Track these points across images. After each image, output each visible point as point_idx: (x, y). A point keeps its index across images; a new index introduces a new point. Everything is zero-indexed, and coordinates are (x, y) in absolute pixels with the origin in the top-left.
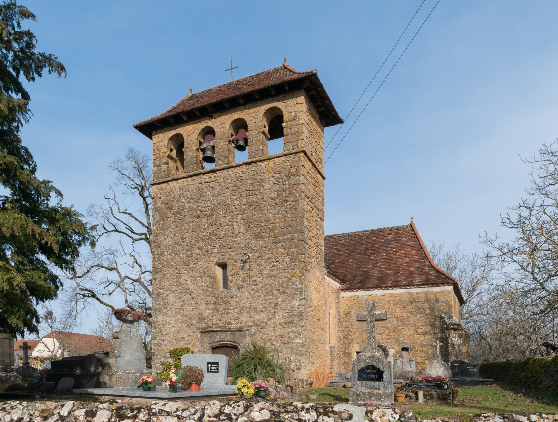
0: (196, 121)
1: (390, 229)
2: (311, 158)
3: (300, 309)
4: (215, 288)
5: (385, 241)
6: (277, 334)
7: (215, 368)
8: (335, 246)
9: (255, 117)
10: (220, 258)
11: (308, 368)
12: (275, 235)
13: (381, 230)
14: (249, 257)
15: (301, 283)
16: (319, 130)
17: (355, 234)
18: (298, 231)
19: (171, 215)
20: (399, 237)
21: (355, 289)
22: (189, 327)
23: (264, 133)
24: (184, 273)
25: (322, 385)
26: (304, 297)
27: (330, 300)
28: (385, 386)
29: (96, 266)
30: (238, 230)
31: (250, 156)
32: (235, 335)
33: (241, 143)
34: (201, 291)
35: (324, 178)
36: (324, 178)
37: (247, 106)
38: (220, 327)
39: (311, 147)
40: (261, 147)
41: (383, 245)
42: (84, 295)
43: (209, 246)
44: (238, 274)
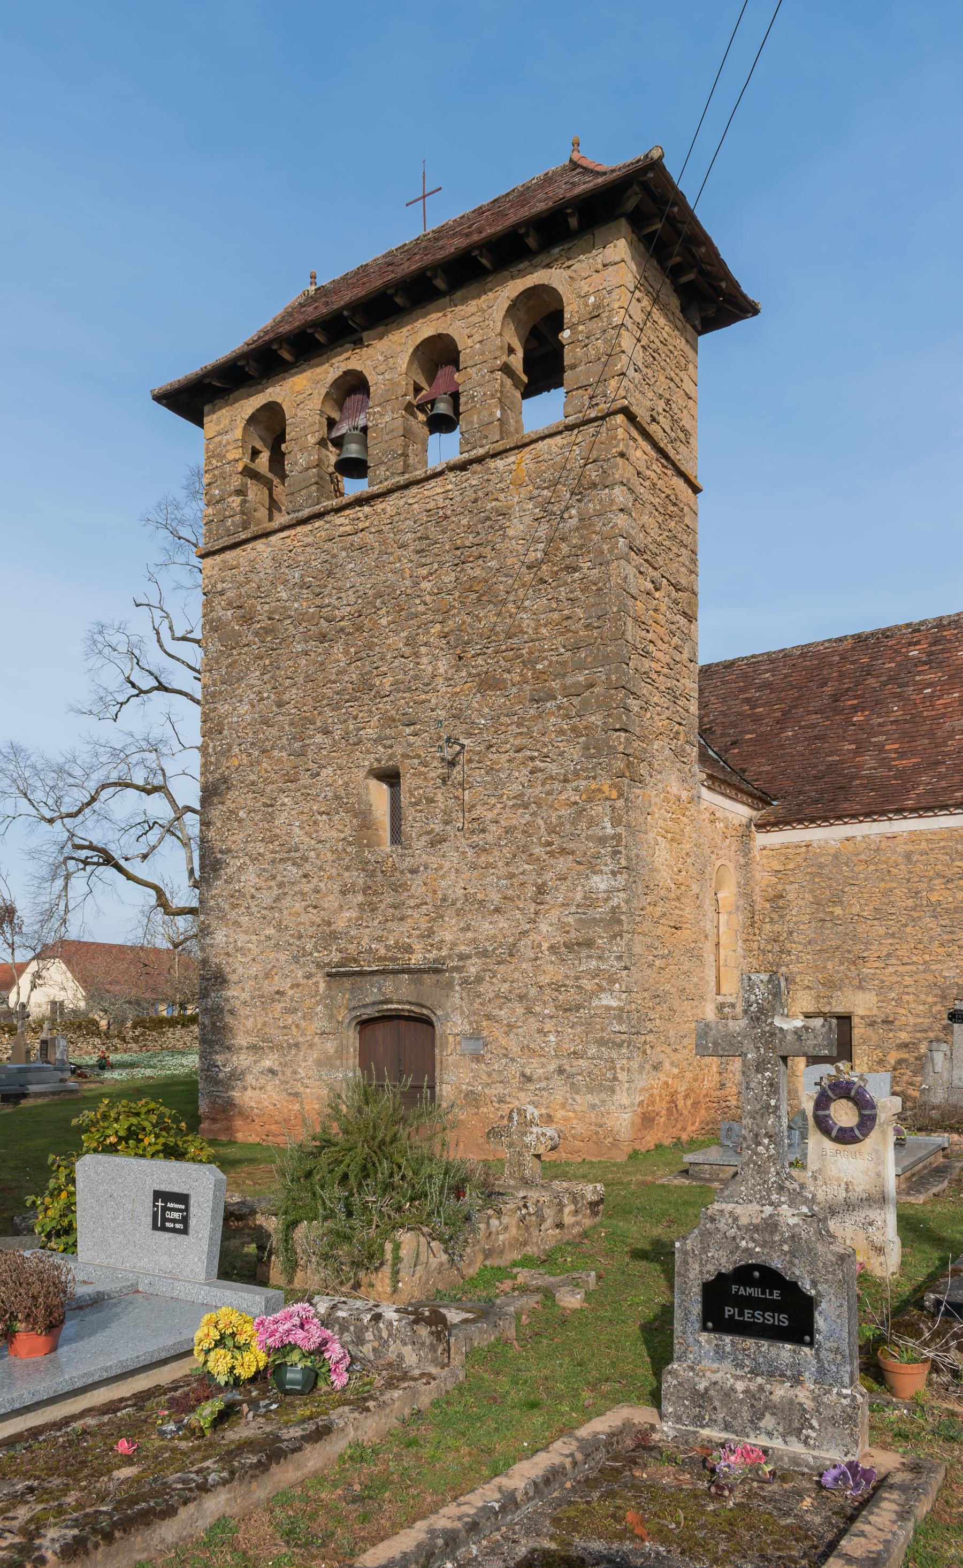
0: (317, 360)
1: (915, 628)
2: (653, 428)
3: (611, 903)
4: (368, 846)
5: (899, 665)
6: (544, 980)
7: (176, 1215)
8: (742, 690)
9: (481, 324)
10: (380, 756)
11: (641, 1084)
12: (538, 676)
13: (886, 634)
14: (463, 746)
15: (616, 822)
16: (681, 343)
17: (805, 652)
18: (605, 660)
19: (250, 638)
20: (943, 651)
21: (800, 821)
22: (296, 960)
23: (506, 369)
24: (283, 804)
25: (690, 1128)
26: (624, 863)
27: (719, 863)
28: (822, 1371)
29: (115, 784)
30: (430, 669)
31: (466, 444)
32: (422, 983)
33: (443, 408)
34: (329, 854)
35: (696, 490)
36: (696, 490)
37: (459, 294)
38: (381, 959)
39: (650, 395)
40: (498, 414)
41: (891, 679)
42: (86, 862)
43: (351, 721)
44: (431, 801)
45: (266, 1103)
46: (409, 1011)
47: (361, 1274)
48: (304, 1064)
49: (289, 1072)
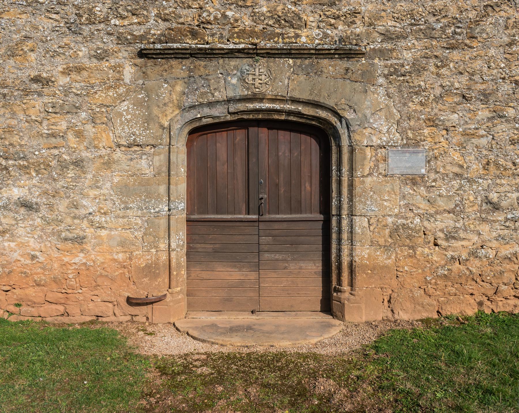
22: (74, 29)
32: (319, 73)
38: (242, 33)
45: (15, 256)
46: (290, 113)
47: (471, 258)
48: (93, 193)
49: (62, 206)
